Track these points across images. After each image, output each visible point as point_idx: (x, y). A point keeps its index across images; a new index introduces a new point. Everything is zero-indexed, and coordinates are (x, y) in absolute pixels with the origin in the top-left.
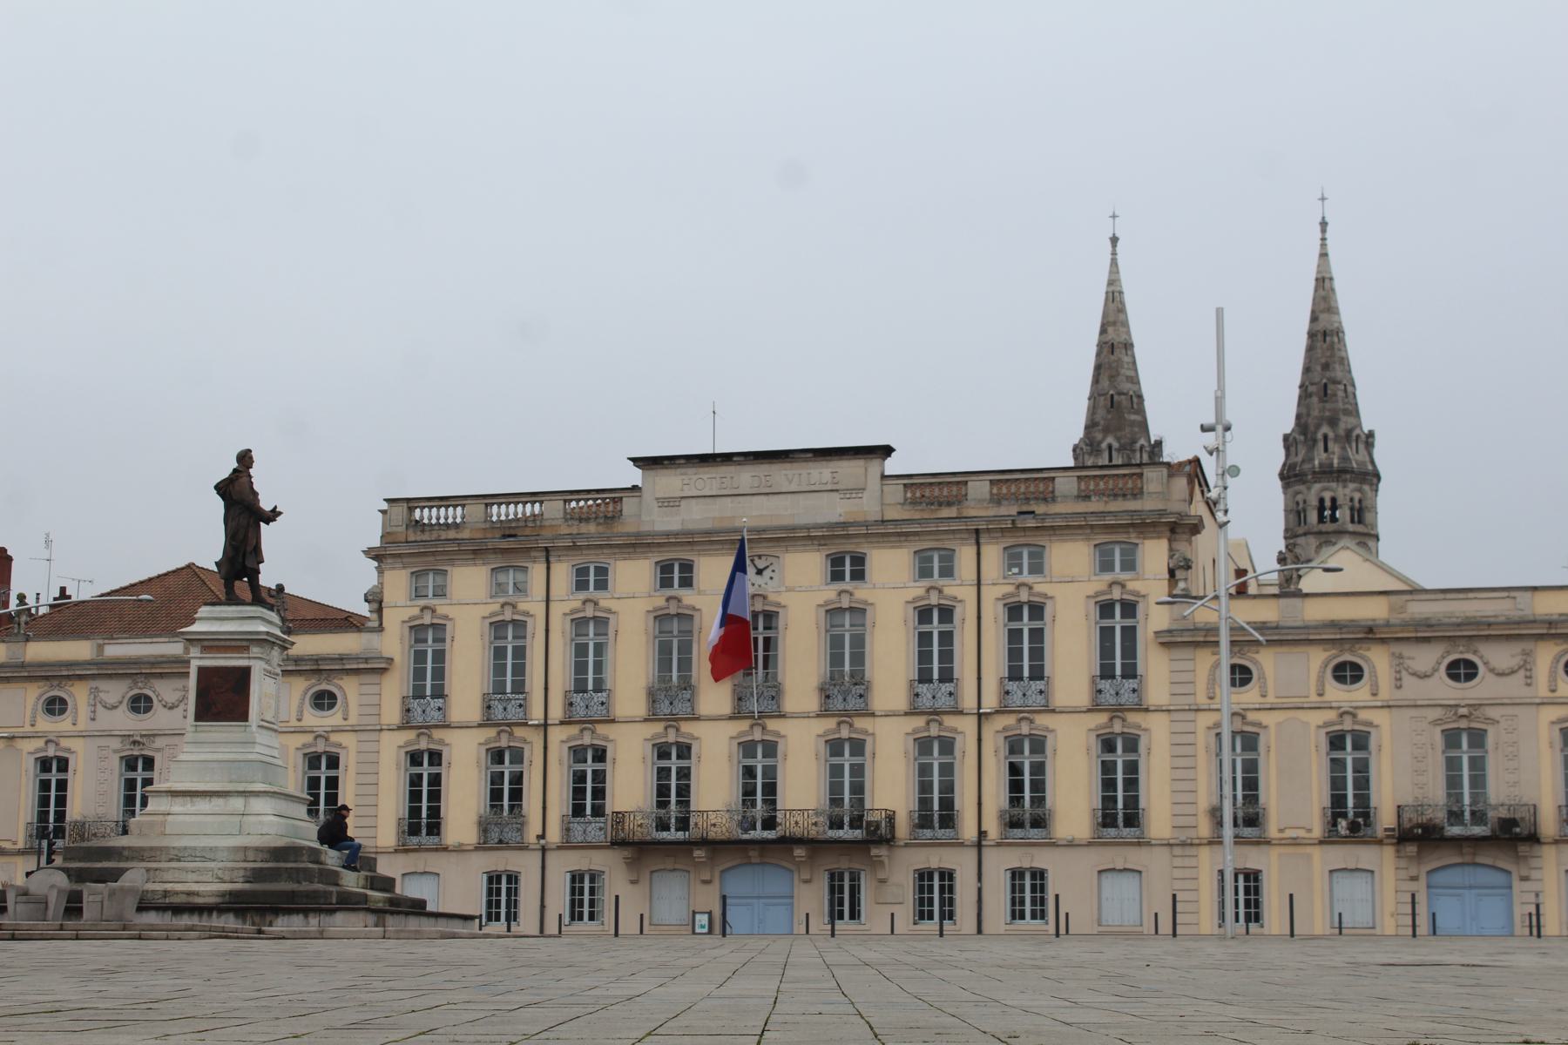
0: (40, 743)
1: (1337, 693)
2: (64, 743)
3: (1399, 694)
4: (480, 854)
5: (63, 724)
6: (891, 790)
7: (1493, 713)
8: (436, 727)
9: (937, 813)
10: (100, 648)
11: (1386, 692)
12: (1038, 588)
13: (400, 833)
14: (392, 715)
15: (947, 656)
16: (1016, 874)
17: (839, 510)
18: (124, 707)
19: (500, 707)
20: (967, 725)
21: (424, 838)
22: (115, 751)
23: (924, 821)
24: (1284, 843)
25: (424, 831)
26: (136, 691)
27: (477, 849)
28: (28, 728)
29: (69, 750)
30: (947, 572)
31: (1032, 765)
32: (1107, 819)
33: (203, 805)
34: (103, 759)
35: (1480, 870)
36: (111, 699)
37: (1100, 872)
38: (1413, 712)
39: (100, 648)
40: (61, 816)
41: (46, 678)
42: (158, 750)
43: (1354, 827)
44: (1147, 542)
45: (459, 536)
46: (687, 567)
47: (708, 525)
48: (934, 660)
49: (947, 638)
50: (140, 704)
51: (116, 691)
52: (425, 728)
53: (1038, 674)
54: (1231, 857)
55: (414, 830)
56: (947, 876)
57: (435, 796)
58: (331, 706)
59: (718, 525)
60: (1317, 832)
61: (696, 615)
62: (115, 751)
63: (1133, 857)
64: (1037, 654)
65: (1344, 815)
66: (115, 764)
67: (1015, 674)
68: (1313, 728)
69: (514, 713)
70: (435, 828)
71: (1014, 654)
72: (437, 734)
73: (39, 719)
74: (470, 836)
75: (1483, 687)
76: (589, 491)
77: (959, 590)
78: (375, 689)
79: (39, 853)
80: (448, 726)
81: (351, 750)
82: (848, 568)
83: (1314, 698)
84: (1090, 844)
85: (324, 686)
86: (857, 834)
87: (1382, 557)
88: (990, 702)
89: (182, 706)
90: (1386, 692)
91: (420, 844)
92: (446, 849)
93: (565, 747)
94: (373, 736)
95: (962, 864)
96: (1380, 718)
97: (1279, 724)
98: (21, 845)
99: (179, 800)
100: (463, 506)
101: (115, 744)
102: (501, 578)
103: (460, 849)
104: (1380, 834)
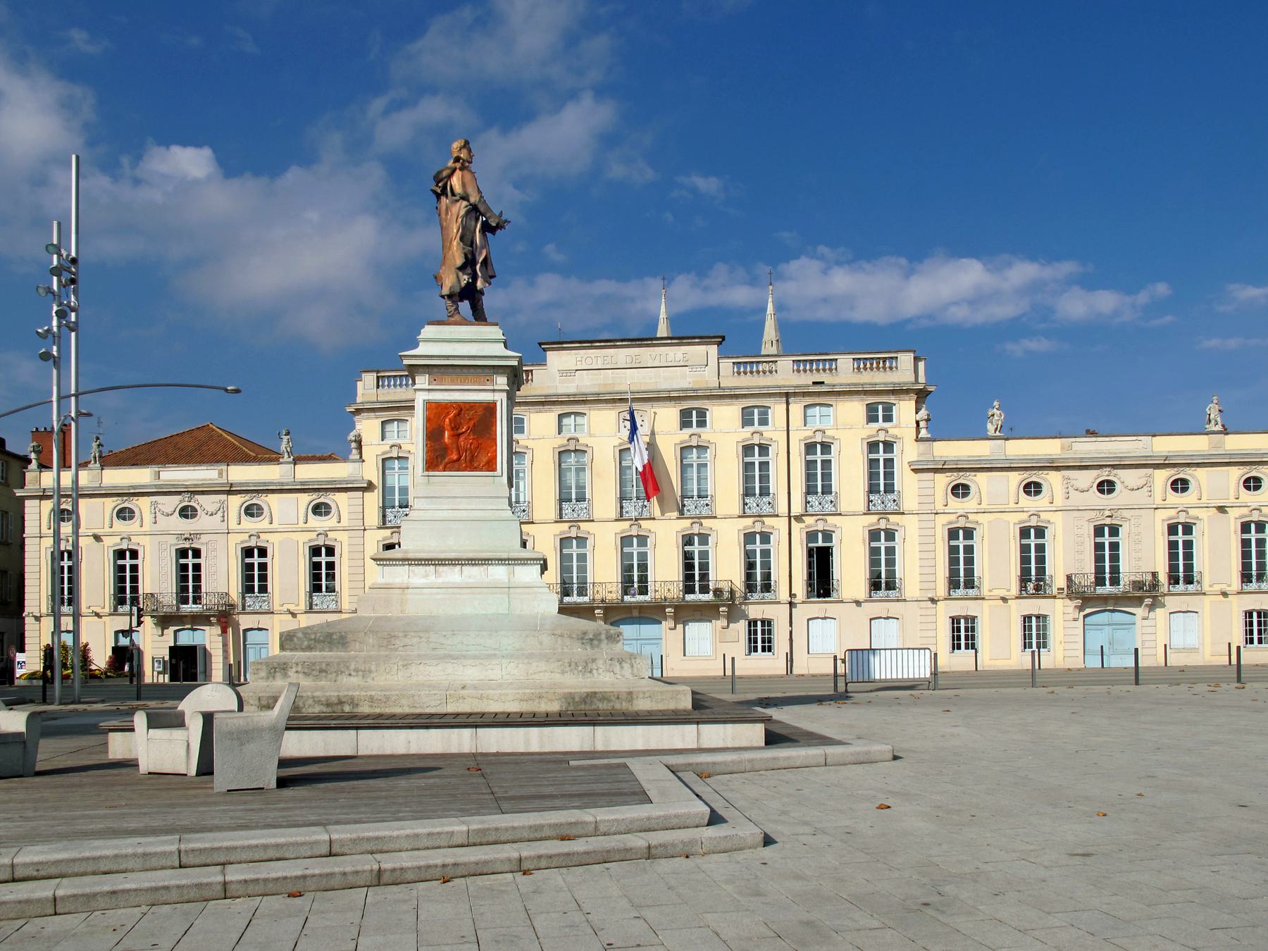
1: (1027, 502)
3: (1069, 502)
6: (727, 569)
7: (1126, 514)
9: (757, 579)
11: (1059, 501)
15: (764, 478)
16: (1027, 619)
17: (689, 380)
20: (781, 524)
23: (750, 587)
25: (1107, 582)
26: (186, 504)
30: (764, 422)
31: (1257, 540)
32: (875, 585)
33: (452, 575)
35: (1117, 614)
38: (1076, 514)
40: (135, 589)
43: (1037, 588)
44: (592, 412)
46: (702, 414)
47: (596, 390)
48: (755, 483)
49: (764, 466)
52: (884, 514)
53: (827, 490)
56: (767, 623)
59: (603, 390)
61: (590, 451)
63: (894, 608)
64: (827, 476)
65: (1030, 580)
67: (810, 490)
71: (810, 477)
75: (202, 523)
77: (773, 432)
79: (131, 615)
81: (343, 543)
82: (880, 413)
83: (1012, 505)
86: (709, 597)
87: (8, 448)
88: (797, 509)
89: (220, 513)
90: (1059, 501)
95: (778, 614)
97: (989, 522)
99: (420, 570)
101: (172, 540)
104: (1055, 592)
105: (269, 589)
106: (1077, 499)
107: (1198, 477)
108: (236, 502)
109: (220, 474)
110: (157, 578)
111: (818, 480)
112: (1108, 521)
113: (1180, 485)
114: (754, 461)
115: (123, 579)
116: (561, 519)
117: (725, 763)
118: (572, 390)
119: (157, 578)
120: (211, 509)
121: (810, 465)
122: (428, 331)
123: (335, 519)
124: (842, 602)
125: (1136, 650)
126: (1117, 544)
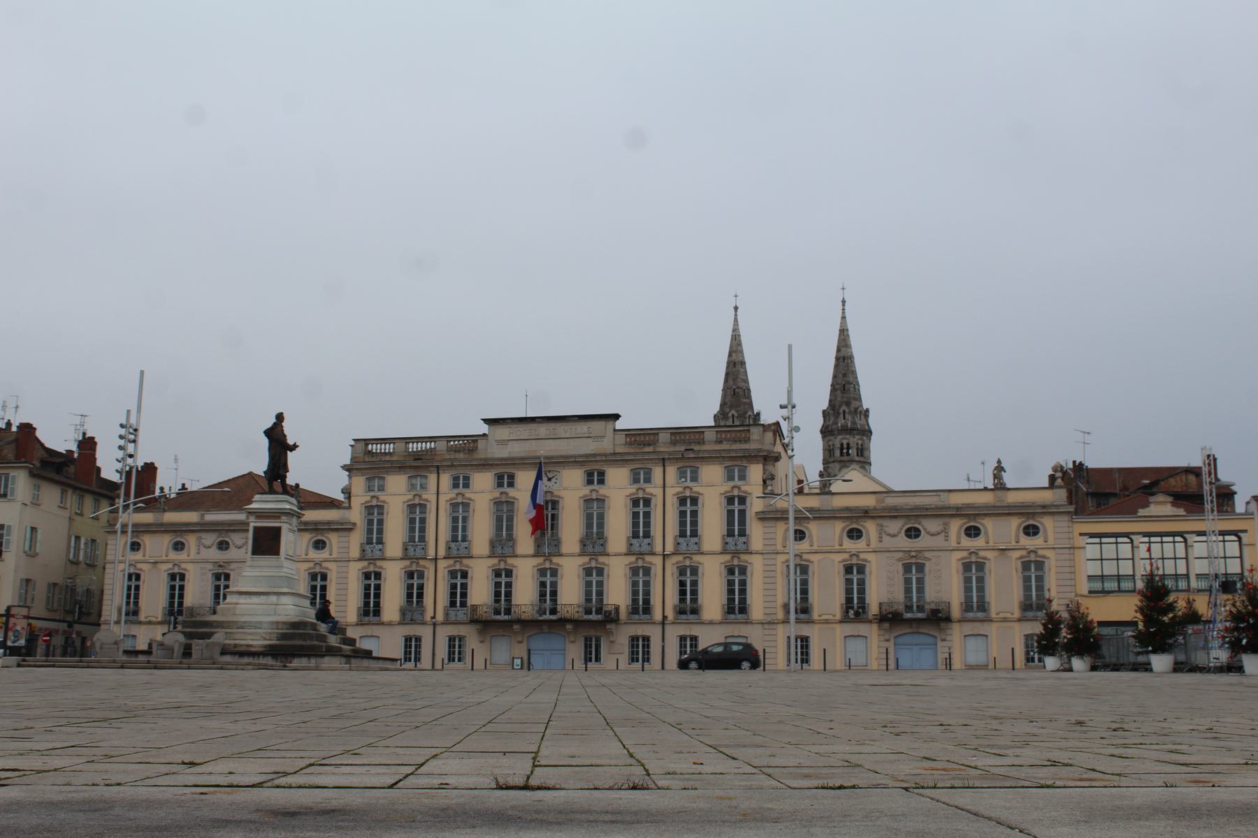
0: (170, 566)
3: (880, 545)
5: (182, 556)
7: (927, 554)
9: (641, 607)
10: (203, 516)
12: (695, 489)
13: (359, 615)
14: (355, 552)
15: (647, 524)
20: (657, 561)
21: (372, 618)
36: (208, 543)
39: (203, 516)
40: (181, 604)
43: (857, 614)
46: (511, 477)
48: (640, 527)
50: (223, 546)
51: (210, 539)
53: (694, 534)
54: (794, 630)
55: (366, 613)
56: (646, 639)
57: (377, 596)
60: (838, 617)
64: (694, 523)
65: (852, 608)
66: (210, 575)
67: (682, 534)
69: (419, 553)
70: (377, 612)
71: (682, 524)
72: (379, 563)
75: (923, 542)
81: (333, 571)
86: (600, 617)
88: (670, 548)
92: (383, 624)
101: (210, 566)
102: (414, 481)
103: (390, 624)
104: (870, 617)
106: (888, 542)
107: (988, 525)
108: (956, 526)
111: (689, 526)
112: (913, 561)
113: (973, 532)
114: (640, 506)
118: (505, 455)
119: (882, 588)
120: (239, 542)
121: (682, 514)
122: (257, 497)
124: (383, 624)
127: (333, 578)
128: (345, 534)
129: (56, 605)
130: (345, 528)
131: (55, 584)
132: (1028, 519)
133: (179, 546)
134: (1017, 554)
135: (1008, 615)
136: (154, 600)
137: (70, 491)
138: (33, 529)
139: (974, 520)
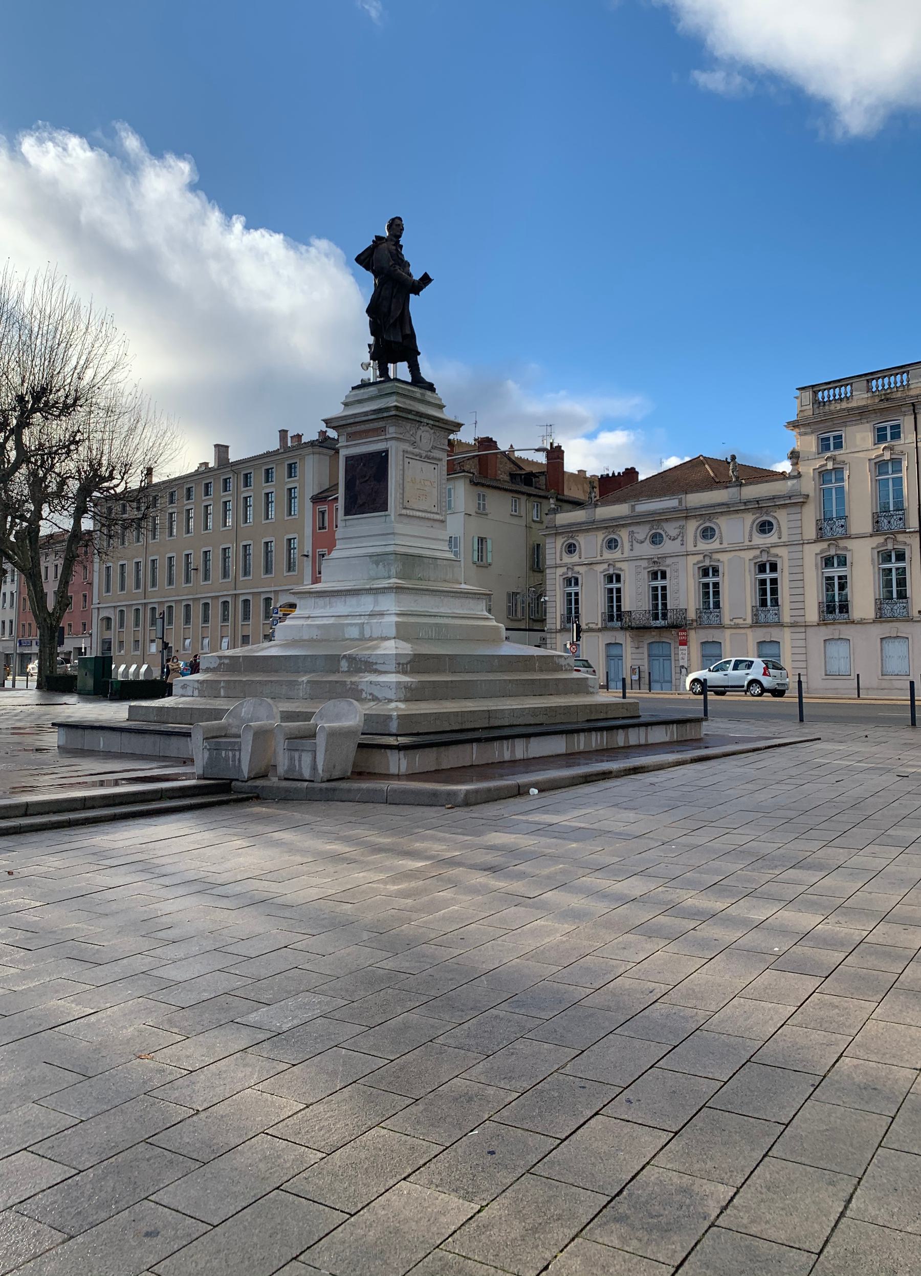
0: (605, 566)
2: (618, 565)
4: (878, 625)
5: (617, 554)
8: (841, 538)
10: (633, 506)
13: (821, 612)
14: (810, 532)
18: (648, 541)
19: (886, 521)
22: (644, 568)
24: (793, 625)
25: (837, 611)
26: (654, 531)
27: (874, 622)
28: (599, 558)
29: (620, 569)
34: (638, 573)
36: (641, 537)
37: (759, 643)
39: (633, 506)
40: (619, 607)
41: (606, 528)
42: (668, 566)
45: (850, 405)
50: (656, 539)
51: (642, 532)
54: (761, 634)
58: (770, 530)
60: (749, 621)
62: (644, 568)
66: (645, 575)
68: (747, 562)
69: (896, 525)
72: (842, 543)
73: (754, 537)
74: (871, 614)
75: (668, 547)
76: (829, 383)
78: (798, 516)
80: (850, 538)
81: (783, 556)
84: (874, 622)
85: (765, 518)
89: (680, 538)
91: (834, 619)
92: (853, 622)
93: (562, 578)
94: (799, 548)
96: (782, 552)
97: (729, 560)
98: (600, 626)
100: (851, 384)
101: (644, 564)
103: (862, 622)
105: (721, 605)
107: (582, 540)
108: (692, 527)
109: (680, 502)
110: (635, 599)
113: (707, 533)
115: (888, 584)
116: (877, 532)
117: (560, 767)
119: (635, 599)
120: (673, 533)
123: (577, 557)
124: (853, 622)
125: (912, 683)
126: (718, 583)
127: (784, 566)
128: (797, 509)
129: (519, 615)
130: (796, 502)
131: (515, 594)
132: (610, 533)
133: (612, 544)
134: (560, 571)
135: (740, 621)
136: (593, 609)
137: (523, 498)
138: (482, 540)
139: (710, 520)
